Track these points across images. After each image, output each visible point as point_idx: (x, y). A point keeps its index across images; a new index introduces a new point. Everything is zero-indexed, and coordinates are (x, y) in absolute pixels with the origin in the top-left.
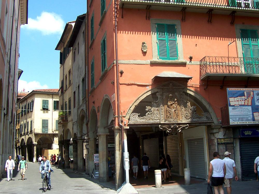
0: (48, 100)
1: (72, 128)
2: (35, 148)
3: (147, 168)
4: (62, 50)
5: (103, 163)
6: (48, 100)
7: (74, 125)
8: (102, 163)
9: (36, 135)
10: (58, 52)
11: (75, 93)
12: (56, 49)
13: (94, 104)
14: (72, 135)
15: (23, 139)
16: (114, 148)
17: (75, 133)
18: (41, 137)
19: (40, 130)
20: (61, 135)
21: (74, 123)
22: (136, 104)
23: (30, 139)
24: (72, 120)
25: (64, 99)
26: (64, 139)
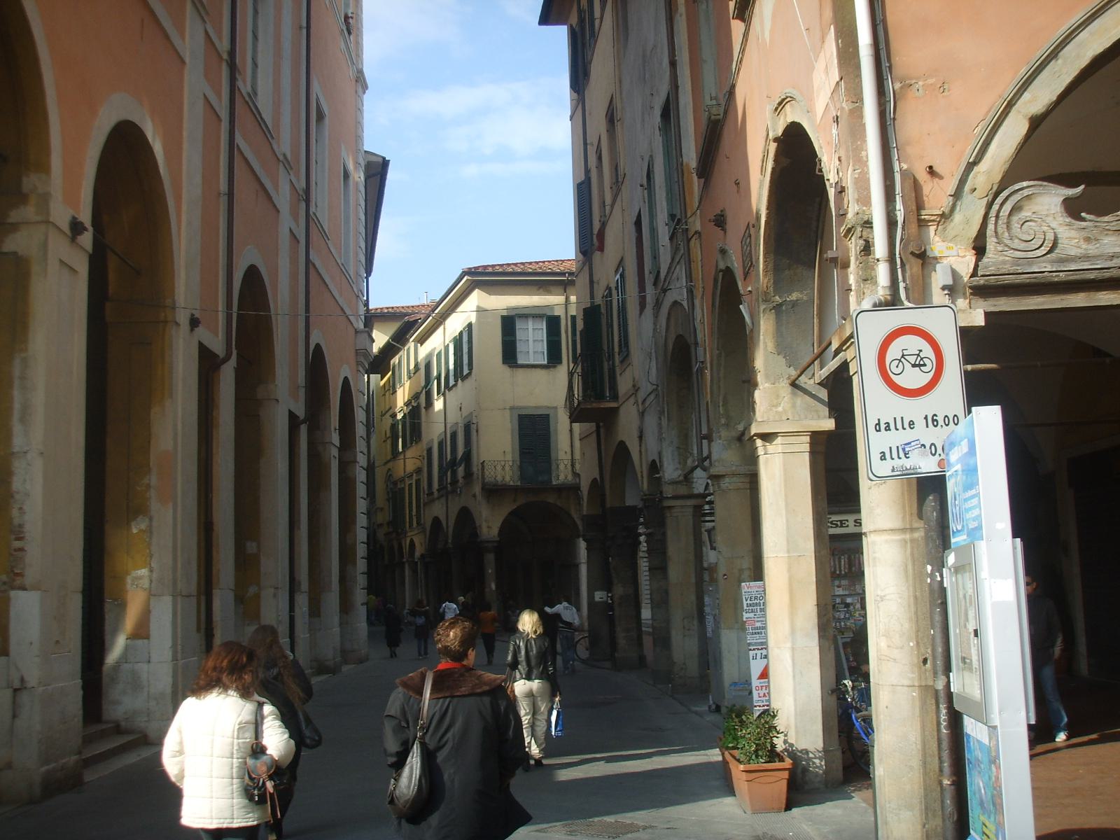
0: (983, 540)
1: (636, 434)
2: (490, 558)
3: (574, 26)
4: (574, 20)
5: (793, 649)
6: (983, 540)
7: (646, 414)
8: (789, 645)
9: (494, 492)
10: (559, 35)
11: (638, 223)
12: (545, 19)
13: (724, 230)
14: (639, 475)
15: (436, 521)
16: (239, 309)
17: (654, 461)
18: (518, 504)
19: (507, 468)
20: (595, 480)
21: (644, 400)
22: (1040, 97)
23: (465, 516)
24: (636, 389)
25: (595, 279)
26: (608, 505)
